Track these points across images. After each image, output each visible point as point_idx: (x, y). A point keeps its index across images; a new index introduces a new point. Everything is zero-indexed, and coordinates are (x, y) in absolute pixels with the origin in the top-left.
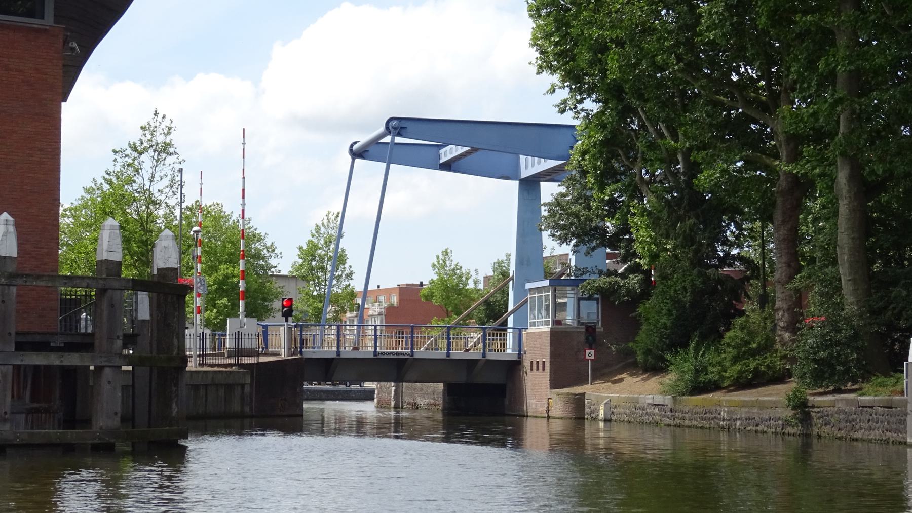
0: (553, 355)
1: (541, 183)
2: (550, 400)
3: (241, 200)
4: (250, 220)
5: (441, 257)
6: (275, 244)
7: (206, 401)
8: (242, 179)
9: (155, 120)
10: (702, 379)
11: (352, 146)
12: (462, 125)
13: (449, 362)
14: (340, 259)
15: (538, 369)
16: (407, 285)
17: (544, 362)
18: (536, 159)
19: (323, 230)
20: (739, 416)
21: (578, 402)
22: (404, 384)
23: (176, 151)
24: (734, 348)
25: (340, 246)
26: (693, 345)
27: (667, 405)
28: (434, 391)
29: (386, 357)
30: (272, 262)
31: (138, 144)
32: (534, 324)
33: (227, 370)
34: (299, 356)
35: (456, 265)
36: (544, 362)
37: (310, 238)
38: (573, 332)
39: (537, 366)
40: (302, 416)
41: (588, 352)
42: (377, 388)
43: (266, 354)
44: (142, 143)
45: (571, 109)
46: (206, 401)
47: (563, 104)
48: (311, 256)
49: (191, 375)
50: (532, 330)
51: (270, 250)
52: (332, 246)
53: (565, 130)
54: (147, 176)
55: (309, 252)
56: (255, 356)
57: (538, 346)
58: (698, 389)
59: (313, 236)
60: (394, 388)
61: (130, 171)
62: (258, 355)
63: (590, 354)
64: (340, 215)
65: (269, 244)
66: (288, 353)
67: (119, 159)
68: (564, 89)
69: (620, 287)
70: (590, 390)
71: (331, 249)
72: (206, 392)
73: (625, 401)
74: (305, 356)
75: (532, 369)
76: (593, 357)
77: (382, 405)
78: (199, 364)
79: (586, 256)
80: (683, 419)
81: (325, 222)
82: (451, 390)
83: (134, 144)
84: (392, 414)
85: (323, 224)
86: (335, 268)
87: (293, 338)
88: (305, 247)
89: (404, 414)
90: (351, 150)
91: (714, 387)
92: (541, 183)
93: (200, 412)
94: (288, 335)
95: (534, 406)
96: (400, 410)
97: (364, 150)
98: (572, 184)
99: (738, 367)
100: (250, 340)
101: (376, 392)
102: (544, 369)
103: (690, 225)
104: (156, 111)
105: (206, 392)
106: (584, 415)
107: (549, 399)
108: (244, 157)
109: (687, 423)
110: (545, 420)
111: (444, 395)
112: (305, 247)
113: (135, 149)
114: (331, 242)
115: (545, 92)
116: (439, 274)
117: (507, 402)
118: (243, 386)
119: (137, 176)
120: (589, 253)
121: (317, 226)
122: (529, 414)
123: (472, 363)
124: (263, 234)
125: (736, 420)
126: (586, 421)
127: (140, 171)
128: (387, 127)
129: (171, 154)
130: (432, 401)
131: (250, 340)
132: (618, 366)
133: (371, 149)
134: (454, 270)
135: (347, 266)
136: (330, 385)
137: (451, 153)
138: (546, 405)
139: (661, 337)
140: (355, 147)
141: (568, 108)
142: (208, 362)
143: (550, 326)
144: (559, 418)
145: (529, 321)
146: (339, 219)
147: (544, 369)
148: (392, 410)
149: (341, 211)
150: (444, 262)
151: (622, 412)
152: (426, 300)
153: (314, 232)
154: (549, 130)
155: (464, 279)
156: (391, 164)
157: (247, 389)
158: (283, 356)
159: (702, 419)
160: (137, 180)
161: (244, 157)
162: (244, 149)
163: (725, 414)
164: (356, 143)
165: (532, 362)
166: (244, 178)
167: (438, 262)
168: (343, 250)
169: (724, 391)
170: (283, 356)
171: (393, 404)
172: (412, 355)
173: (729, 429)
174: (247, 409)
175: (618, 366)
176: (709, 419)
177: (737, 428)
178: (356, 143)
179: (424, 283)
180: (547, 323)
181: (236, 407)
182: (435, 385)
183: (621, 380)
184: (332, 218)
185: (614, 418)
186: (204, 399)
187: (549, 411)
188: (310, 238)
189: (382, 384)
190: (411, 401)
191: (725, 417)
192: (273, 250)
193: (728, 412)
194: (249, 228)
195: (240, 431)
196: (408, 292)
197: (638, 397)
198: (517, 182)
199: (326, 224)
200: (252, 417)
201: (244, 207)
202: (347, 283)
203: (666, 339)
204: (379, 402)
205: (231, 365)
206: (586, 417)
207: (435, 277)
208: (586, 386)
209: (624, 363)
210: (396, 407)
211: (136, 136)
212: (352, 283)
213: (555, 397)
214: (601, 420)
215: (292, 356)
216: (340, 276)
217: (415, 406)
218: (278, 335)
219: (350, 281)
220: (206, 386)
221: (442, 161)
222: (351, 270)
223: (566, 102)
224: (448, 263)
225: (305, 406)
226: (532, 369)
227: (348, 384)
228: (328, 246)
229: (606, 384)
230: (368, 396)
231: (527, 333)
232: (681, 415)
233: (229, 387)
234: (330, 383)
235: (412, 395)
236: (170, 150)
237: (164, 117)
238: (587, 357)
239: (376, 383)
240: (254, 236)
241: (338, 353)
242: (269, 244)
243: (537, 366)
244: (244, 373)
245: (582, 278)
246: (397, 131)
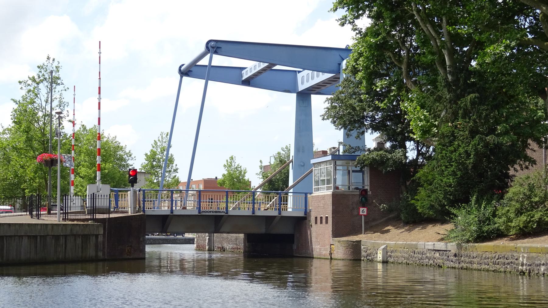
0: (334, 212)
1: (312, 96)
2: (332, 246)
3: (98, 95)
4: (116, 137)
5: (229, 161)
6: (132, 152)
7: (65, 248)
8: (98, 80)
9: (48, 62)
10: (485, 229)
11: (180, 67)
12: (261, 46)
13: (254, 218)
14: (170, 160)
15: (321, 223)
16: (208, 179)
17: (327, 217)
18: (315, 72)
19: (159, 144)
20: (543, 262)
21: (356, 248)
22: (215, 234)
23: (62, 82)
24: (517, 201)
25: (170, 153)
26: (474, 199)
27: (450, 251)
28: (236, 239)
29: (207, 214)
30: (130, 162)
31: (36, 77)
32: (318, 189)
33: (84, 223)
34: (142, 213)
35: (238, 165)
36: (327, 217)
37: (152, 148)
38: (349, 195)
39: (321, 220)
40: (144, 259)
41: (361, 209)
42: (196, 237)
43: (116, 212)
44: (39, 77)
45: (350, 23)
46: (65, 248)
47: (343, 19)
48: (153, 158)
49: (53, 228)
50: (315, 194)
51: (128, 155)
52: (165, 153)
53: (334, 52)
54: (43, 99)
55: (152, 157)
56: (106, 213)
57: (322, 205)
58: (482, 237)
59: (153, 147)
60: (208, 238)
61: (32, 95)
62: (109, 212)
63: (363, 211)
64: (169, 134)
65: (127, 152)
66: (134, 211)
67: (24, 87)
68: (344, 8)
69: (388, 159)
70: (362, 237)
71: (165, 155)
72: (66, 241)
73: (403, 247)
74: (147, 213)
75: (316, 223)
76: (365, 213)
77: (200, 248)
78: (63, 219)
79: (357, 139)
80: (471, 263)
81: (160, 139)
82: (250, 238)
83: (34, 77)
84: (207, 256)
85: (159, 140)
86: (167, 166)
87: (138, 199)
88: (149, 154)
89: (214, 256)
90: (180, 70)
91: (499, 235)
92: (312, 96)
93: (60, 257)
94: (134, 199)
95: (318, 250)
96: (213, 252)
97: (188, 70)
98: (348, 84)
99: (523, 218)
100: (103, 200)
101: (195, 240)
102: (327, 222)
103: (471, 99)
104: (48, 57)
105: (66, 241)
106: (361, 257)
107: (331, 245)
108: (100, 63)
109: (475, 266)
110: (328, 262)
111: (244, 243)
112: (149, 154)
113: (34, 80)
114: (164, 150)
115: (329, 10)
116: (228, 171)
117: (295, 247)
118: (97, 236)
119: (37, 98)
120: (358, 137)
121: (155, 141)
122: (315, 256)
123: (269, 219)
124: (124, 146)
125: (540, 265)
126: (362, 261)
127: (38, 96)
128: (207, 47)
129: (59, 84)
130: (235, 246)
131: (103, 200)
132: (382, 220)
133: (193, 69)
134: (237, 167)
135: (174, 165)
136: (165, 235)
137: (251, 72)
138: (329, 250)
139: (446, 193)
140: (182, 68)
141: (347, 22)
142: (69, 217)
143: (332, 190)
144: (340, 260)
145: (313, 187)
146: (168, 136)
147: (327, 222)
148: (207, 252)
149: (169, 131)
150: (231, 163)
151: (400, 256)
152: (221, 185)
153: (154, 145)
154: (324, 52)
155: (243, 173)
156: (209, 81)
157: (100, 239)
158: (130, 213)
159: (494, 264)
160: (37, 102)
161: (100, 63)
162: (100, 57)
163: (525, 260)
164: (183, 65)
165: (316, 218)
166: (100, 79)
167: (228, 163)
168: (172, 156)
169: (506, 239)
170: (130, 214)
171: (207, 247)
172: (227, 213)
173: (530, 272)
174: (100, 254)
175: (382, 220)
176: (504, 264)
177: (541, 273)
178: (183, 65)
179: (218, 178)
180: (328, 189)
181: (91, 252)
182: (237, 235)
183: (388, 231)
184: (164, 136)
185: (391, 260)
186: (64, 246)
187: (331, 254)
188: (152, 148)
189: (200, 234)
190: (220, 246)
191: (525, 262)
192: (130, 155)
193: (528, 258)
194: (116, 142)
195: (95, 273)
196: (209, 183)
197: (417, 245)
198: (294, 95)
199: (161, 140)
200: (104, 260)
201: (100, 101)
202: (174, 175)
203: (450, 195)
204: (197, 246)
205: (87, 220)
206: (362, 259)
207: (226, 173)
208: (361, 236)
209: (386, 218)
210: (209, 250)
211: (34, 73)
212: (178, 175)
213: (337, 244)
214: (379, 262)
215: (137, 213)
216: (170, 171)
217: (223, 250)
218: (126, 201)
219: (176, 174)
220: (66, 236)
221: (243, 79)
222: (177, 167)
223: (346, 17)
224: (233, 164)
225: (149, 249)
226: (316, 223)
227: (175, 235)
228: (162, 153)
229: (376, 234)
230: (190, 241)
231: (312, 196)
232: (467, 260)
233: (86, 238)
234: (165, 234)
235: (221, 242)
236: (58, 81)
237: (54, 60)
238: (361, 213)
239: (196, 234)
240: (119, 147)
241: (172, 211)
242: (127, 152)
243: (321, 220)
244: (98, 227)
245: (354, 154)
246: (215, 49)
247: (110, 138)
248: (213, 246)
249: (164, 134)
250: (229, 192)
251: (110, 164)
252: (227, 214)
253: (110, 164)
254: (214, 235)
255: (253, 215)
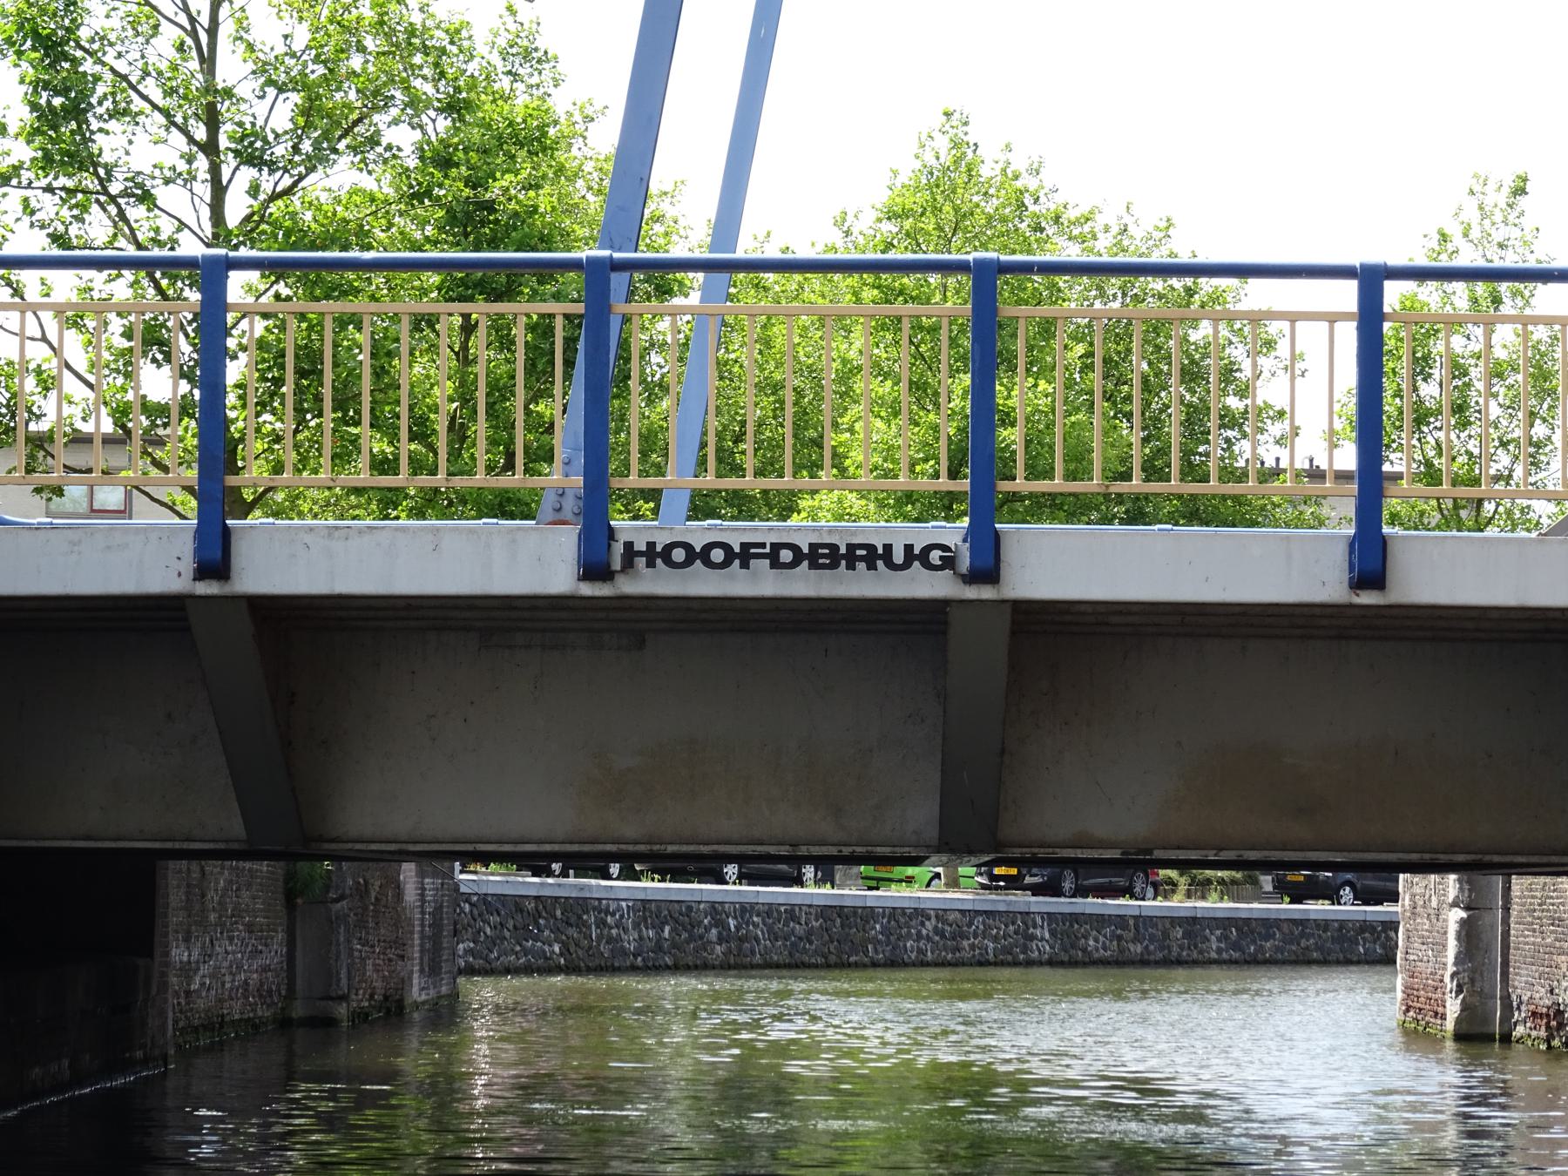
29: (702, 584)
81: (1471, 214)
247: (1132, 229)
248: (1507, 999)
249: (1492, 186)
250: (618, 281)
251: (1042, 385)
252: (986, 593)
253: (1042, 385)
254: (1507, 889)
255: (1367, 598)
